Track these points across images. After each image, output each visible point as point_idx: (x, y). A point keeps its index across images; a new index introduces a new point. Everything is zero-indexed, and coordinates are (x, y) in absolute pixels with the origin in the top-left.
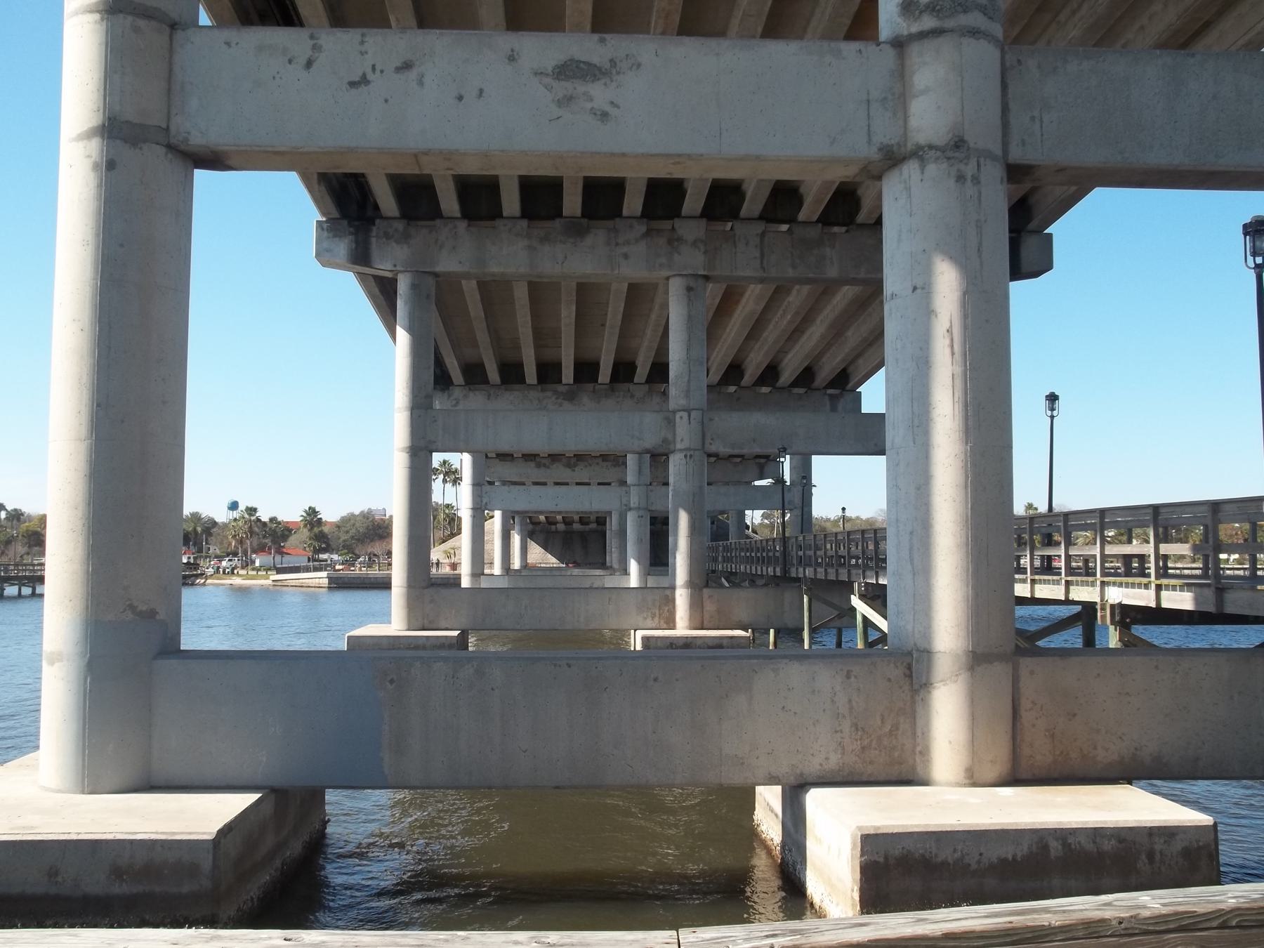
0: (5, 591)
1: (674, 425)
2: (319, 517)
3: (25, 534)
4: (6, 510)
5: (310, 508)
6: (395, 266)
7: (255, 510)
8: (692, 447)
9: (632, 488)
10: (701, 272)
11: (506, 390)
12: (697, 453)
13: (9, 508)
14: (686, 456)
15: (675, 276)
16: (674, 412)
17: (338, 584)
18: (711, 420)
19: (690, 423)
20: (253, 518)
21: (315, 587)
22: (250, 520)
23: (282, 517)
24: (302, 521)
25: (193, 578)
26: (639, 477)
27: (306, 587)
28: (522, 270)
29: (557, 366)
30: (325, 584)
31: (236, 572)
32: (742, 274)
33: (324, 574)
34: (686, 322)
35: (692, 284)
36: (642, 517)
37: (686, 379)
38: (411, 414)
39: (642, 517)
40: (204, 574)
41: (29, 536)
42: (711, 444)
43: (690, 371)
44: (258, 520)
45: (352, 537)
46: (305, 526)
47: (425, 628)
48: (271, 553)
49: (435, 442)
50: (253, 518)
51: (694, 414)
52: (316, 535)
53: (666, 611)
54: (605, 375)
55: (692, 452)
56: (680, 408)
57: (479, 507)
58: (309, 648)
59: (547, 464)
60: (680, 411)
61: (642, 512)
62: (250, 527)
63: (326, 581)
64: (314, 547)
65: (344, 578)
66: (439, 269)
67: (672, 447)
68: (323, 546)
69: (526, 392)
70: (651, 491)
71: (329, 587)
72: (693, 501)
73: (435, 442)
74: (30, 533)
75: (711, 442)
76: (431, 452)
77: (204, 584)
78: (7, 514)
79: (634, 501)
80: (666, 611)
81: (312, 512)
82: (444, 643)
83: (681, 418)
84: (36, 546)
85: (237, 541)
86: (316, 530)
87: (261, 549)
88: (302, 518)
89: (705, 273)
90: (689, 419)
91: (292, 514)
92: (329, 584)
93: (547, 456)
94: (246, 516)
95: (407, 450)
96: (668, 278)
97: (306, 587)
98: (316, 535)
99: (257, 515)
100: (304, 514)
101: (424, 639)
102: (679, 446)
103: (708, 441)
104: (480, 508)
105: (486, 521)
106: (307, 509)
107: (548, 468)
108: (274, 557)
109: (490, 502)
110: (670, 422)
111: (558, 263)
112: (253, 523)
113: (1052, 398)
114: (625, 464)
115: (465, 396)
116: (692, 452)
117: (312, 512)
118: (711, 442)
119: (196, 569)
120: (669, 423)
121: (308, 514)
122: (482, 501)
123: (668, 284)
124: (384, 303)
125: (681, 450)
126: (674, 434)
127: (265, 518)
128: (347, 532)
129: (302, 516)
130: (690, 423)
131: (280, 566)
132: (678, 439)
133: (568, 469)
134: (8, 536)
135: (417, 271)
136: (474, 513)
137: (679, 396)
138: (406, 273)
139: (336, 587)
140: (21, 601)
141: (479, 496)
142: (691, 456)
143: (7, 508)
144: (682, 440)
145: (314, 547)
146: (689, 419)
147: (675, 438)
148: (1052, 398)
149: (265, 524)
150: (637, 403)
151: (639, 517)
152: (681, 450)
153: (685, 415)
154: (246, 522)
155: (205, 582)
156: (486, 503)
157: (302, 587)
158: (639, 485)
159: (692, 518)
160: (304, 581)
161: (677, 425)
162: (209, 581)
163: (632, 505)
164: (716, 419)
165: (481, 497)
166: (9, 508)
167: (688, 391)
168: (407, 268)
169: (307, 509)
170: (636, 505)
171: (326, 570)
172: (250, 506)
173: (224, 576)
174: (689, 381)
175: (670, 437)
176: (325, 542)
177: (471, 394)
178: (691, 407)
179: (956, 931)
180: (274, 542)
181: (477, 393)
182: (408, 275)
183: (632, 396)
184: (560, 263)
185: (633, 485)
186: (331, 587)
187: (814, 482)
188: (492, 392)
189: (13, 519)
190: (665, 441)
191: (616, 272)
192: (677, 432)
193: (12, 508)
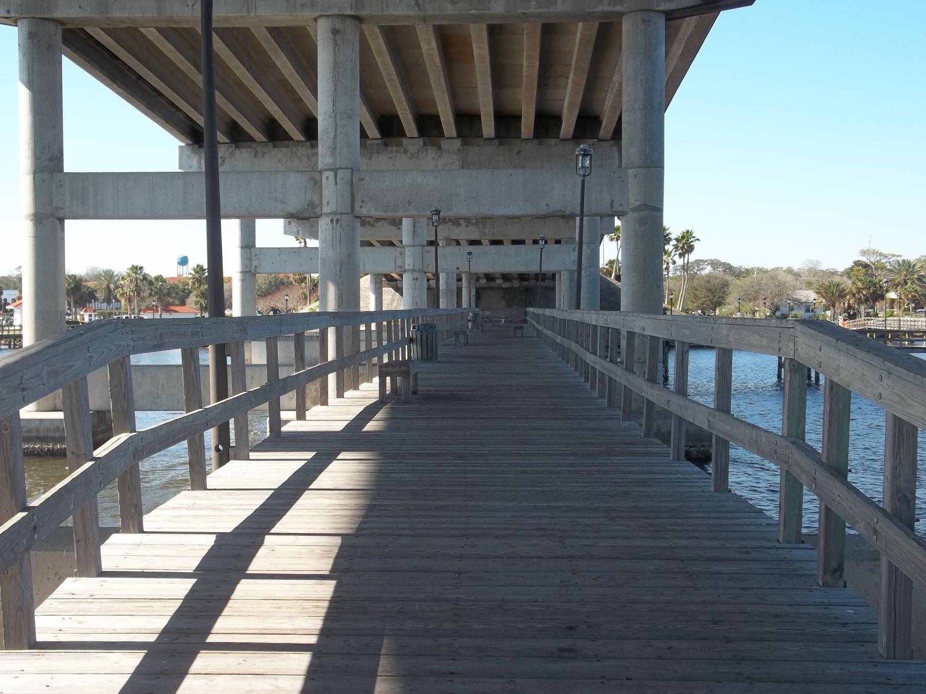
1: (321, 188)
5: (198, 266)
6: (9, 12)
7: (141, 268)
8: (338, 211)
9: (406, 248)
10: (348, 12)
11: (274, 146)
12: (344, 216)
14: (332, 221)
15: (321, 16)
16: (321, 172)
18: (362, 180)
19: (336, 183)
26: (414, 238)
28: (148, 14)
29: (558, 119)
32: (394, 13)
34: (331, 70)
35: (339, 26)
36: (417, 279)
37: (333, 134)
38: (34, 178)
39: (417, 279)
42: (361, 207)
43: (336, 126)
47: (58, 408)
48: (158, 311)
49: (62, 208)
51: (340, 173)
53: (313, 390)
54: (568, 127)
55: (339, 217)
56: (326, 168)
57: (248, 270)
58: (159, 413)
59: (372, 222)
60: (326, 170)
61: (416, 275)
62: (137, 285)
64: (201, 305)
66: (57, 15)
67: (318, 211)
69: (295, 149)
70: (427, 252)
72: (340, 270)
73: (62, 208)
75: (362, 204)
76: (61, 221)
79: (409, 263)
80: (313, 390)
82: (58, 427)
83: (327, 178)
89: (353, 13)
90: (336, 179)
93: (310, 219)
95: (31, 218)
96: (316, 20)
98: (202, 293)
101: (38, 423)
102: (326, 210)
103: (358, 204)
104: (250, 272)
105: (361, 277)
107: (373, 226)
109: (260, 265)
110: (317, 184)
111: (187, 6)
112: (139, 281)
114: (401, 223)
115: (232, 154)
116: (339, 217)
118: (362, 204)
120: (315, 184)
121: (196, 272)
122: (251, 264)
123: (316, 26)
124: (76, 56)
125: (327, 214)
126: (321, 197)
130: (336, 183)
132: (325, 202)
133: (393, 227)
135: (34, 18)
136: (243, 276)
137: (325, 154)
138: (23, 20)
141: (248, 259)
142: (338, 221)
144: (328, 203)
145: (201, 305)
146: (336, 179)
147: (321, 200)
150: (411, 159)
151: (414, 279)
152: (327, 214)
153: (331, 174)
154: (131, 280)
156: (256, 266)
158: (413, 246)
159: (339, 289)
161: (324, 186)
163: (407, 267)
164: (367, 179)
165: (250, 260)
167: (334, 148)
168: (22, 14)
169: (196, 267)
170: (411, 267)
172: (135, 265)
174: (335, 137)
175: (316, 200)
177: (238, 152)
178: (338, 167)
180: (160, 300)
181: (244, 150)
182: (25, 22)
183: (406, 152)
184: (190, 5)
185: (409, 246)
188: (259, 150)
190: (311, 204)
191: (253, 14)
192: (323, 194)
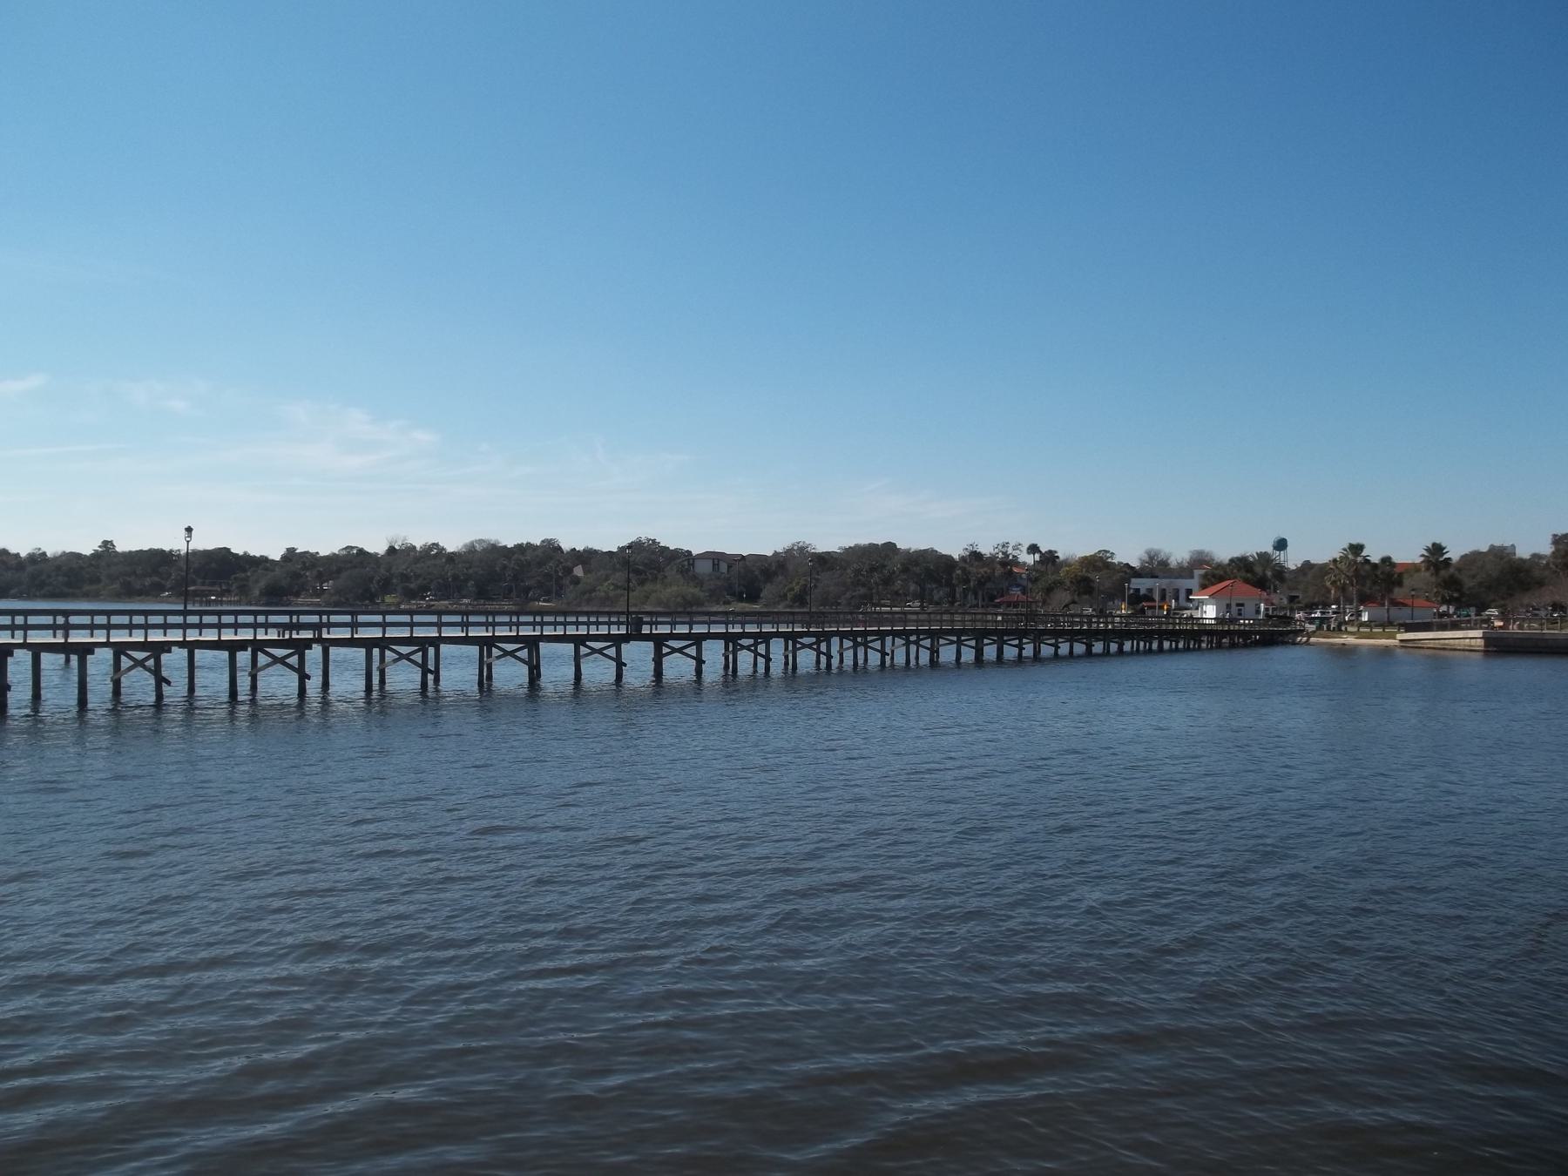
0: (1093, 648)
2: (1446, 556)
3: (1074, 581)
4: (1040, 552)
13: (1043, 550)
17: (1498, 647)
20: (1359, 559)
21: (1463, 650)
22: (1355, 562)
23: (1398, 558)
24: (1422, 562)
25: (1291, 635)
27: (1451, 650)
30: (1479, 646)
31: (1343, 628)
33: (1478, 633)
40: (1303, 631)
41: (1079, 582)
44: (1367, 562)
45: (1480, 584)
46: (1428, 569)
48: (1383, 605)
50: (1359, 559)
52: (1445, 582)
63: (1481, 642)
65: (1507, 638)
68: (1456, 595)
71: (1485, 651)
74: (1079, 578)
77: (1307, 643)
78: (1040, 557)
81: (1437, 549)
84: (1086, 594)
85: (1337, 587)
86: (1443, 573)
87: (1365, 599)
88: (1422, 559)
91: (1408, 553)
92: (1485, 646)
94: (1350, 556)
97: (1451, 650)
98: (1445, 582)
99: (1363, 554)
100: (1426, 554)
106: (1430, 546)
108: (1388, 610)
113: (189, 530)
117: (1437, 549)
119: (1289, 624)
127: (1375, 559)
128: (1474, 577)
129: (1423, 556)
131: (1411, 621)
134: (1050, 582)
139: (1496, 651)
140: (1107, 659)
143: (1041, 549)
145: (1443, 597)
148: (189, 530)
149: (1375, 566)
155: (1308, 640)
157: (1444, 649)
160: (1447, 642)
162: (1313, 640)
166: (1043, 550)
171: (1481, 628)
173: (1330, 634)
176: (1457, 590)
179: (110, 602)
186: (1488, 651)
187: (88, 547)
189: (1048, 563)
193: (1047, 550)
